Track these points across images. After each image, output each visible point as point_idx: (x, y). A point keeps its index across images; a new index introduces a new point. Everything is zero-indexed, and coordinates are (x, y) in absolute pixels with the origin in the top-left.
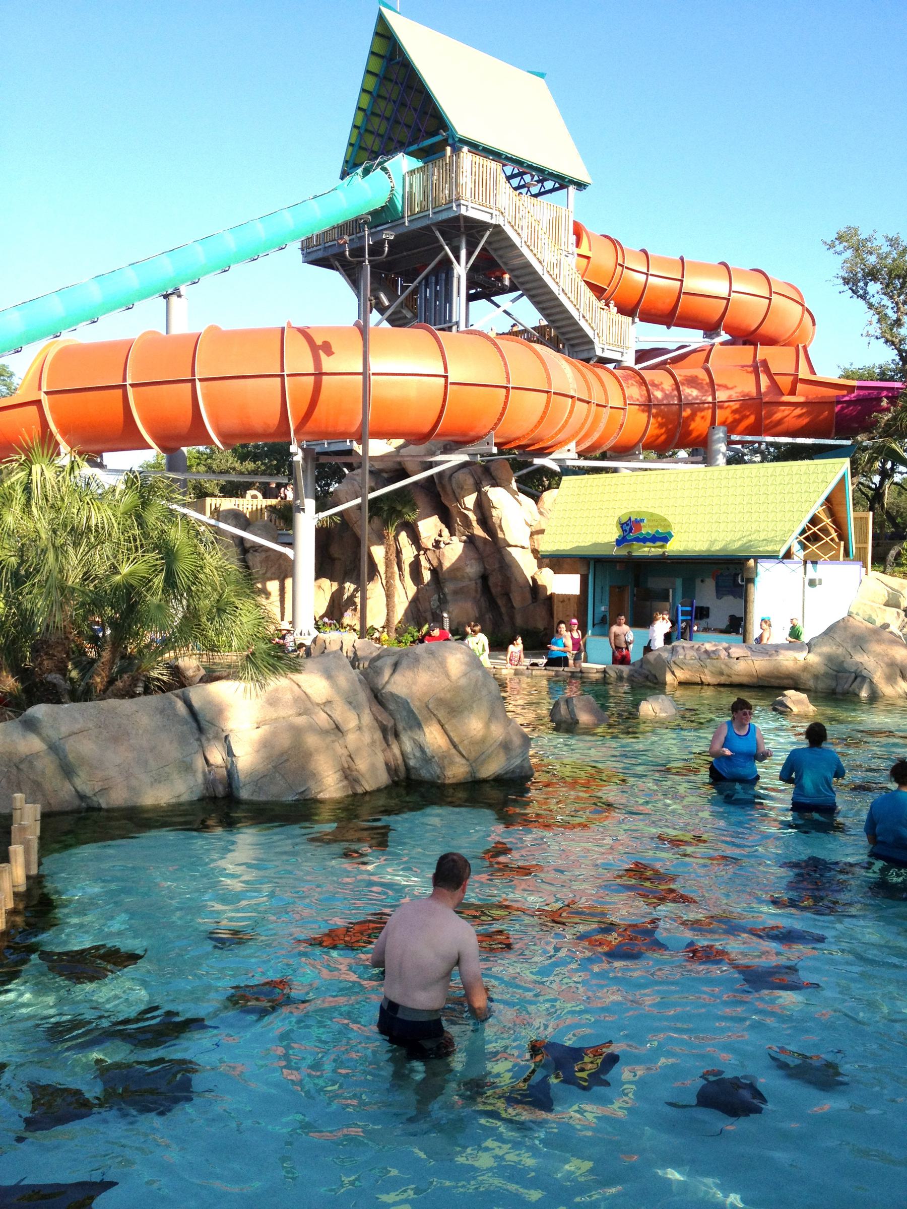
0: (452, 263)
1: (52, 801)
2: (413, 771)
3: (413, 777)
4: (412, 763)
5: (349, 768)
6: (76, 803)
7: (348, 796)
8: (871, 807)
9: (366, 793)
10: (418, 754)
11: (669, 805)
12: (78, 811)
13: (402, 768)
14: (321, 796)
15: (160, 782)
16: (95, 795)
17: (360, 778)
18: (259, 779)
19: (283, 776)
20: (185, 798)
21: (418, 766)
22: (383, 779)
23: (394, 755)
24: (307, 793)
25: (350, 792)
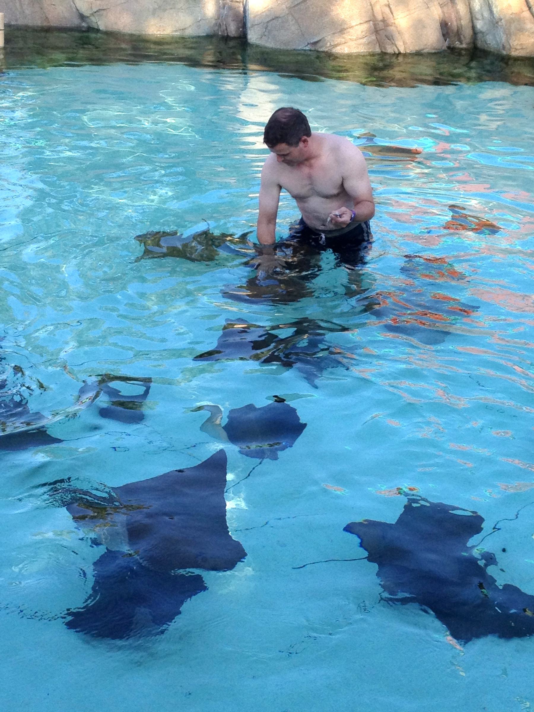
0: (75, 629)
1: (50, 16)
2: (479, 36)
3: (479, 44)
4: (479, 25)
5: (384, 21)
6: (76, 22)
7: (373, 55)
8: (421, 341)
9: (398, 55)
10: (486, 14)
11: (217, 174)
12: (77, 29)
13: (467, 33)
14: (338, 50)
15: (165, 10)
16: (92, 14)
17: (396, 35)
18: (272, 21)
19: (297, 21)
20: (190, 32)
21: (484, 30)
22: (431, 38)
23: (457, 12)
24: (320, 44)
25: (378, 50)
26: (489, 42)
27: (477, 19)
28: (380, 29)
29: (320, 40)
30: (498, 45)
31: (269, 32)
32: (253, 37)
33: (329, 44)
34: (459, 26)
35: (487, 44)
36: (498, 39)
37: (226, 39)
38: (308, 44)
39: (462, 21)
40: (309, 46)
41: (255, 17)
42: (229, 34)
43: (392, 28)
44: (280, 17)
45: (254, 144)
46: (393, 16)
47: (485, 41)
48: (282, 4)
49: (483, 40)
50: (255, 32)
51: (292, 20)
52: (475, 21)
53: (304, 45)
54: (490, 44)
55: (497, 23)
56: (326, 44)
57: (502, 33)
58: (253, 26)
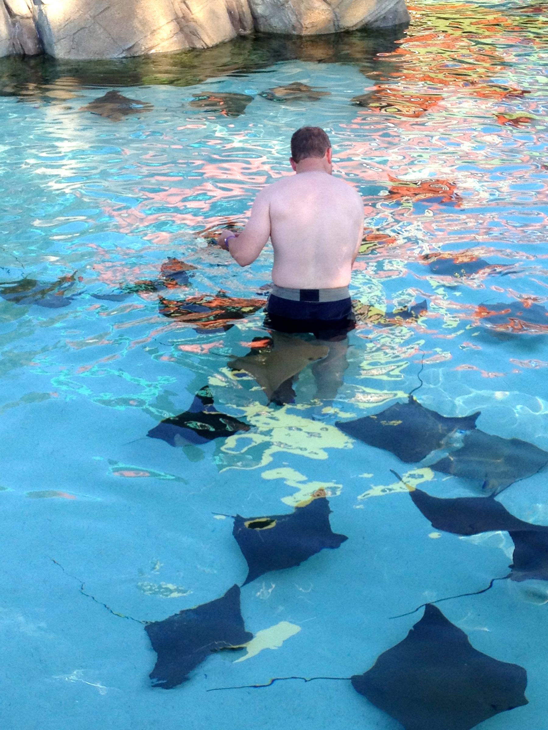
2: (261, 21)
4: (260, 10)
5: (184, 17)
18: (77, 31)
21: (267, 13)
24: (135, 49)
26: (274, 25)
27: (257, 4)
28: (184, 25)
29: (133, 46)
30: (286, 26)
31: (77, 44)
32: (60, 51)
33: (143, 48)
34: (241, 13)
35: (271, 27)
36: (286, 21)
37: (24, 57)
38: (124, 51)
39: (243, 8)
40: (124, 52)
41: (59, 31)
42: (26, 53)
43: (193, 24)
44: (86, 28)
45: (240, 141)
46: (191, 11)
47: (270, 25)
48: (85, 14)
49: (266, 23)
50: (61, 46)
51: (100, 29)
52: (254, 7)
53: (119, 53)
54: (275, 27)
55: (283, 5)
56: (141, 48)
57: (290, 15)
58: (59, 40)
